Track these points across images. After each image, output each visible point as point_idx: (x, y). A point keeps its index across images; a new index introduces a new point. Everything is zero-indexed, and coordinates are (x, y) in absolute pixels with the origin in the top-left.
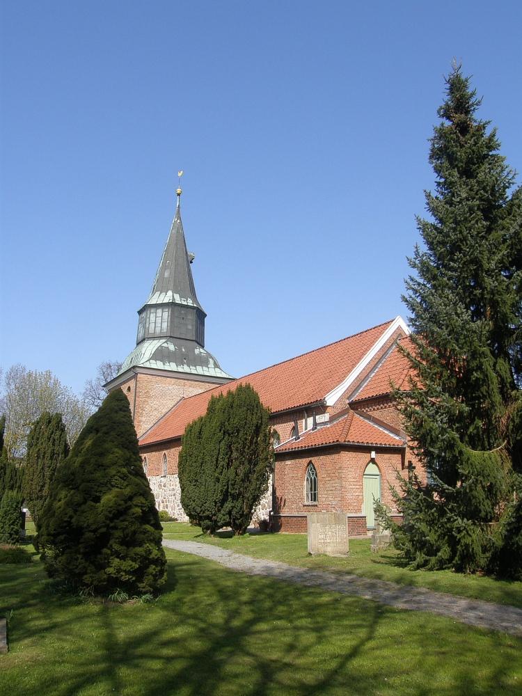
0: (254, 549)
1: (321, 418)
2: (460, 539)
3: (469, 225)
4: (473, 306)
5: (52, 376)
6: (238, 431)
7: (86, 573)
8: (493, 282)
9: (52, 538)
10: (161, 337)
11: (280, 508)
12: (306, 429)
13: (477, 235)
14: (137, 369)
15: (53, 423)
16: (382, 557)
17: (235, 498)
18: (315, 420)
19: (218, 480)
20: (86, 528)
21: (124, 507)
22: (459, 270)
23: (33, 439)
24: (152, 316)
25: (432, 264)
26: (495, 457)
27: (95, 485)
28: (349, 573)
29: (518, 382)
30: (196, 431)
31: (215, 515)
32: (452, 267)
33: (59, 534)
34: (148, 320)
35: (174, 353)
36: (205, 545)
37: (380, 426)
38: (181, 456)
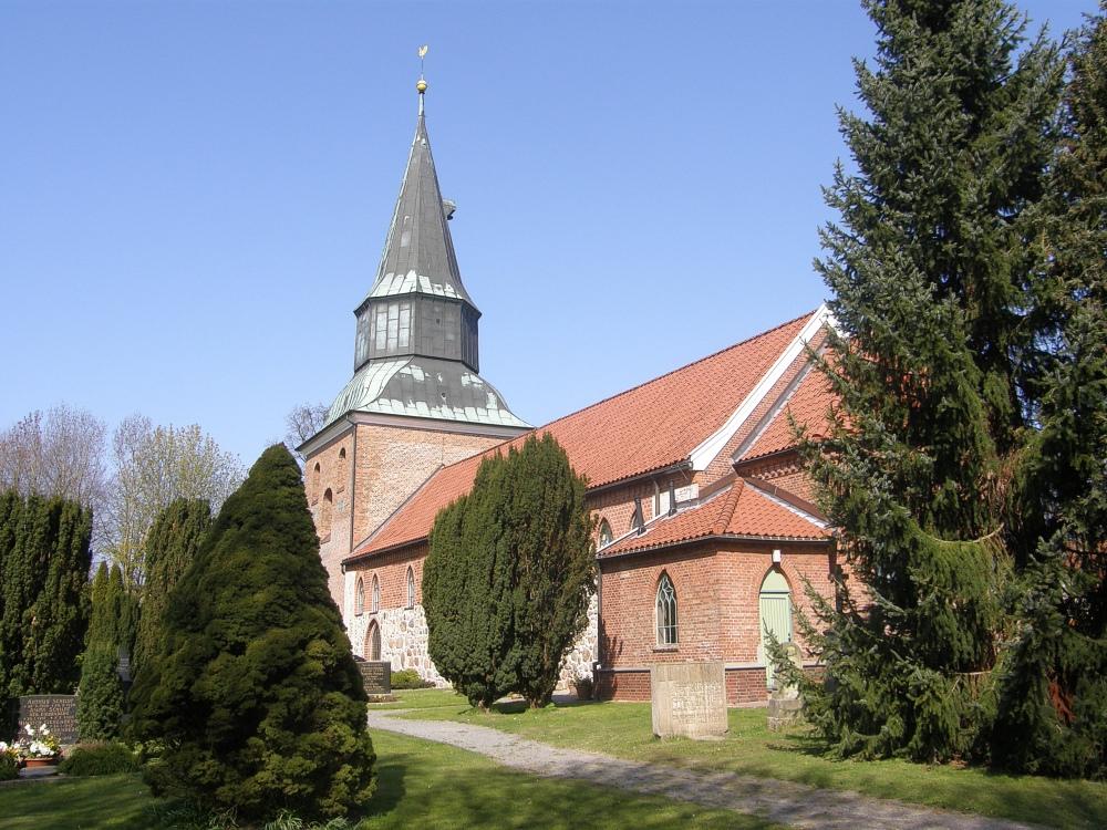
0: (558, 731)
1: (683, 494)
2: (919, 707)
3: (934, 120)
4: (945, 277)
5: (203, 433)
6: (528, 520)
7: (222, 783)
8: (975, 228)
9: (156, 723)
10: (398, 357)
11: (613, 656)
12: (658, 513)
13: (949, 139)
14: (357, 416)
15: (193, 516)
16: (789, 737)
17: (526, 640)
18: (672, 497)
19: (494, 609)
20: (218, 701)
21: (290, 660)
22: (913, 206)
23: (156, 547)
24: (381, 319)
25: (868, 198)
26: (982, 552)
27: (235, 623)
28: (720, 768)
29: (1030, 415)
30: (454, 522)
31: (490, 673)
32: (903, 201)
33: (167, 716)
34: (373, 325)
35: (424, 384)
36: (472, 728)
37: (791, 504)
38: (427, 569)
